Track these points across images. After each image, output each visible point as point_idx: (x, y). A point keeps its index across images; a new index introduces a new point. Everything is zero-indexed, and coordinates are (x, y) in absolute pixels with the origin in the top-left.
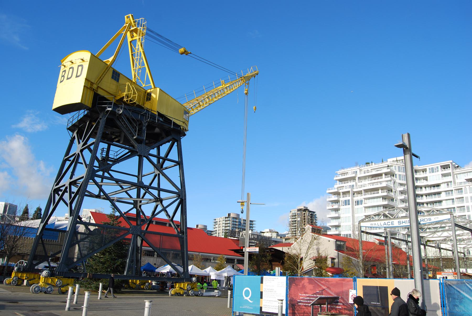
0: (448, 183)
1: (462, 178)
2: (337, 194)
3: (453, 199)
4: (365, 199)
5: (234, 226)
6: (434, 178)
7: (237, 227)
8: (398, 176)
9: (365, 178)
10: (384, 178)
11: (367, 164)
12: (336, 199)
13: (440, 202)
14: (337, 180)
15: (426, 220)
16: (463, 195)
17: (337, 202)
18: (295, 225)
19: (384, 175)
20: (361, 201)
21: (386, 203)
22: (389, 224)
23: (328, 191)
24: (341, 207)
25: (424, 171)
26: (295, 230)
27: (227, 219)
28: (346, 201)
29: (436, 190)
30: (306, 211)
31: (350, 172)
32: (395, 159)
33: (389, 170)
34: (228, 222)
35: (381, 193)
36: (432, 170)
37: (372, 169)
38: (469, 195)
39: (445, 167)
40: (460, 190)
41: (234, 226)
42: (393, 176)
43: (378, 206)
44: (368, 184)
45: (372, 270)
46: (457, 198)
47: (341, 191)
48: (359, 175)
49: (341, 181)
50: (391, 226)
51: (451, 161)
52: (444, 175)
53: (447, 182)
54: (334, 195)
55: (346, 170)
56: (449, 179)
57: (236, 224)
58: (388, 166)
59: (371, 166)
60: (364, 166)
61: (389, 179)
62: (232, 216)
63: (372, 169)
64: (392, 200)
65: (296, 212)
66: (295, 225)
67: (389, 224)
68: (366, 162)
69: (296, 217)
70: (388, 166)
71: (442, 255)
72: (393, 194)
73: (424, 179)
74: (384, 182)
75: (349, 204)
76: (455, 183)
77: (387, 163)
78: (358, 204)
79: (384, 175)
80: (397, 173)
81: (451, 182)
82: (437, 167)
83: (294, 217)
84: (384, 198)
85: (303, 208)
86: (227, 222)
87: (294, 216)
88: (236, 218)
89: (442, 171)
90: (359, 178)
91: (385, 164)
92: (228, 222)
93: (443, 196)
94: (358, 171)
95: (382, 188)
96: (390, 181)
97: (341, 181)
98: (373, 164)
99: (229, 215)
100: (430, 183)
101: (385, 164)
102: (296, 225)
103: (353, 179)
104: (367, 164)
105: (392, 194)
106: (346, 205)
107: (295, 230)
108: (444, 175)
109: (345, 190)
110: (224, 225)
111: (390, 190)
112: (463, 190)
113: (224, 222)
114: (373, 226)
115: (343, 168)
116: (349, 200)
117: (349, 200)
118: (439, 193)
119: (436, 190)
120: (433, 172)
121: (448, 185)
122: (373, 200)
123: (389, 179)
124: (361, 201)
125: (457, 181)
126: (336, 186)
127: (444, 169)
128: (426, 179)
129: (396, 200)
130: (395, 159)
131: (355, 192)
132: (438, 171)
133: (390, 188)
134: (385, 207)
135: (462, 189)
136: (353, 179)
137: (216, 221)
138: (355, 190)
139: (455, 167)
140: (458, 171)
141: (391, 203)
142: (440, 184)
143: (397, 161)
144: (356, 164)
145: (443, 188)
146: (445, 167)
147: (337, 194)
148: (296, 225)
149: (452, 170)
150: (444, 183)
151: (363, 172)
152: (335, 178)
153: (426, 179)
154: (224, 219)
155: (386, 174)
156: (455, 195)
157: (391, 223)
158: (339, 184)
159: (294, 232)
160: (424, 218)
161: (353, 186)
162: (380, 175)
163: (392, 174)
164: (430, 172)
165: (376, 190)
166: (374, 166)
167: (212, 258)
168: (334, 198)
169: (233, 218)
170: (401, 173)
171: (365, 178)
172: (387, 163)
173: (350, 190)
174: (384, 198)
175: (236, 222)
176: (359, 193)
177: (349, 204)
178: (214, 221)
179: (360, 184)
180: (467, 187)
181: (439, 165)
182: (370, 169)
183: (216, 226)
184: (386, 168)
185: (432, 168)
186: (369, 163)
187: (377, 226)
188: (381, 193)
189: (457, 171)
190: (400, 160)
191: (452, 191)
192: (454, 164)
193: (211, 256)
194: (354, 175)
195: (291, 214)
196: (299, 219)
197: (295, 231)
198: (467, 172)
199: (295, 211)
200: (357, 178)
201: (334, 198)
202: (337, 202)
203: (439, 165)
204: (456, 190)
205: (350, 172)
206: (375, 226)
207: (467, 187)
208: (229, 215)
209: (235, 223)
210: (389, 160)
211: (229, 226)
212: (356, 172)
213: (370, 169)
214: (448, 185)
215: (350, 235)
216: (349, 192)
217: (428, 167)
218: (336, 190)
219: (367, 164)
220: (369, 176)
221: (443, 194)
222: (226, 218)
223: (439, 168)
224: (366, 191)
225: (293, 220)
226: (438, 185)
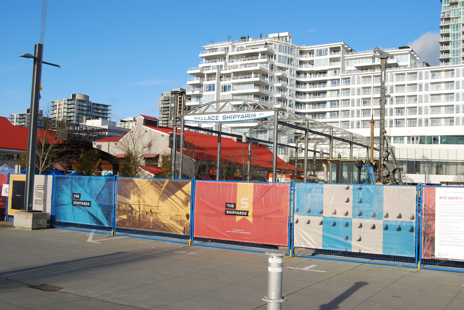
0: (335, 70)
1: (352, 66)
2: (201, 75)
3: (338, 90)
4: (233, 84)
5: (80, 112)
6: (321, 62)
7: (85, 113)
8: (277, 57)
9: (238, 57)
10: (260, 59)
11: (242, 38)
12: (198, 82)
13: (324, 92)
14: (202, 57)
15: (251, 116)
16: (350, 86)
17: (199, 86)
18: (167, 112)
19: (260, 55)
20: (229, 87)
21: (257, 90)
22: (213, 118)
23: (189, 72)
24: (205, 93)
25: (311, 52)
26: (166, 119)
27: (70, 102)
28: (210, 85)
29: (322, 78)
30: (182, 95)
31: (220, 48)
32: (276, 35)
33: (266, 49)
34: (72, 106)
35: (253, 78)
36: (320, 53)
37: (246, 47)
38: (461, 79)
39: (335, 50)
40: (347, 80)
41: (80, 112)
42: (272, 57)
43: (248, 94)
44: (240, 65)
45: (211, 171)
46: (344, 89)
47: (205, 72)
48: (230, 53)
49: (209, 58)
50: (215, 120)
51: (342, 43)
52: (332, 60)
53: (335, 69)
54: (197, 76)
55: (215, 45)
56: (338, 65)
57: (83, 110)
58: (266, 44)
59: (247, 42)
60: (239, 41)
61: (266, 60)
62: (78, 97)
63: (246, 47)
64: (267, 87)
65: (170, 95)
66: (167, 112)
67: (213, 118)
68: (241, 36)
69: (170, 102)
70: (266, 44)
71: (354, 155)
72: (268, 80)
73: (309, 63)
74: (260, 63)
75: (214, 90)
76: (343, 70)
77: (266, 40)
78: (225, 90)
79: (260, 55)
80: (277, 53)
81: (339, 69)
82: (326, 50)
83: (166, 102)
84: (256, 84)
85: (179, 90)
86: (70, 107)
87: (167, 100)
88: (83, 101)
89: (331, 54)
90: (230, 56)
91: (263, 40)
92: (72, 106)
93: (329, 86)
94: (230, 47)
95: (256, 72)
96: (267, 63)
97: (209, 58)
98: (250, 39)
99: (74, 96)
100: (315, 68)
101: (263, 41)
102: (169, 112)
103: (222, 57)
104: (243, 38)
105: (268, 80)
106: (210, 90)
107: (166, 119)
108: (332, 60)
109: (211, 71)
110: (66, 110)
111: (265, 75)
112: (351, 79)
113: (66, 106)
114: (197, 120)
115: (212, 42)
116: (214, 85)
117: (214, 85)
118: (324, 82)
119: (322, 78)
120: (321, 55)
121: (335, 72)
122: (243, 86)
123: (266, 60)
124: (229, 87)
125: (347, 68)
126: (201, 66)
127: (335, 52)
128: (311, 63)
129: (271, 88)
130: (276, 35)
131: (223, 74)
132: (326, 54)
133: (265, 72)
134: (256, 95)
135: (349, 78)
136: (222, 57)
137: (55, 104)
138: (223, 72)
139: (348, 51)
140: (349, 56)
141: (265, 91)
142: (327, 70)
143: (279, 37)
144: (229, 38)
145: (329, 76)
146: (335, 50)
147: (201, 75)
148: (169, 112)
149: (343, 54)
150: (332, 69)
151: (236, 49)
152: (201, 55)
153: (311, 63)
154: (66, 102)
155: (263, 54)
156: (341, 86)
157: (215, 118)
158: (204, 64)
159: (166, 122)
160: (249, 113)
161: (221, 66)
162: (256, 54)
163: (269, 55)
164: (317, 55)
165: (248, 73)
166: (251, 42)
167: (15, 155)
168: (196, 81)
169: (80, 101)
170: (281, 54)
171: (238, 57)
172: (266, 40)
173: (215, 71)
174: (256, 84)
175: (83, 106)
176: (228, 75)
177: (214, 90)
178: (51, 104)
179: (231, 64)
180: (356, 76)
181: (328, 46)
182: (245, 46)
183: (55, 111)
184: (263, 46)
185: (321, 50)
186: (245, 38)
187: (201, 120)
188: (253, 78)
189: (350, 55)
190: (282, 37)
191: (339, 80)
192: (346, 46)
193: (15, 153)
194: (223, 52)
195: (162, 98)
196: (173, 105)
197: (168, 121)
198: (359, 58)
199: (168, 94)
200: (227, 57)
201: (196, 81)
202: (199, 86)
203: (328, 46)
204: (344, 79)
205: (220, 48)
206: (199, 120)
207: (356, 76)
208: (74, 96)
209: (81, 108)
210: (271, 36)
211: (73, 112)
212: (228, 48)
213: (245, 46)
214: (335, 72)
215: (212, 128)
216: (215, 74)
217: (316, 48)
218: (198, 71)
219: (242, 38)
220: (242, 55)
221: (329, 83)
222: (68, 100)
223: (329, 50)
224: (237, 74)
225: (165, 106)
226: (324, 72)
